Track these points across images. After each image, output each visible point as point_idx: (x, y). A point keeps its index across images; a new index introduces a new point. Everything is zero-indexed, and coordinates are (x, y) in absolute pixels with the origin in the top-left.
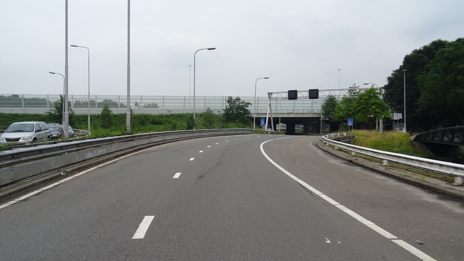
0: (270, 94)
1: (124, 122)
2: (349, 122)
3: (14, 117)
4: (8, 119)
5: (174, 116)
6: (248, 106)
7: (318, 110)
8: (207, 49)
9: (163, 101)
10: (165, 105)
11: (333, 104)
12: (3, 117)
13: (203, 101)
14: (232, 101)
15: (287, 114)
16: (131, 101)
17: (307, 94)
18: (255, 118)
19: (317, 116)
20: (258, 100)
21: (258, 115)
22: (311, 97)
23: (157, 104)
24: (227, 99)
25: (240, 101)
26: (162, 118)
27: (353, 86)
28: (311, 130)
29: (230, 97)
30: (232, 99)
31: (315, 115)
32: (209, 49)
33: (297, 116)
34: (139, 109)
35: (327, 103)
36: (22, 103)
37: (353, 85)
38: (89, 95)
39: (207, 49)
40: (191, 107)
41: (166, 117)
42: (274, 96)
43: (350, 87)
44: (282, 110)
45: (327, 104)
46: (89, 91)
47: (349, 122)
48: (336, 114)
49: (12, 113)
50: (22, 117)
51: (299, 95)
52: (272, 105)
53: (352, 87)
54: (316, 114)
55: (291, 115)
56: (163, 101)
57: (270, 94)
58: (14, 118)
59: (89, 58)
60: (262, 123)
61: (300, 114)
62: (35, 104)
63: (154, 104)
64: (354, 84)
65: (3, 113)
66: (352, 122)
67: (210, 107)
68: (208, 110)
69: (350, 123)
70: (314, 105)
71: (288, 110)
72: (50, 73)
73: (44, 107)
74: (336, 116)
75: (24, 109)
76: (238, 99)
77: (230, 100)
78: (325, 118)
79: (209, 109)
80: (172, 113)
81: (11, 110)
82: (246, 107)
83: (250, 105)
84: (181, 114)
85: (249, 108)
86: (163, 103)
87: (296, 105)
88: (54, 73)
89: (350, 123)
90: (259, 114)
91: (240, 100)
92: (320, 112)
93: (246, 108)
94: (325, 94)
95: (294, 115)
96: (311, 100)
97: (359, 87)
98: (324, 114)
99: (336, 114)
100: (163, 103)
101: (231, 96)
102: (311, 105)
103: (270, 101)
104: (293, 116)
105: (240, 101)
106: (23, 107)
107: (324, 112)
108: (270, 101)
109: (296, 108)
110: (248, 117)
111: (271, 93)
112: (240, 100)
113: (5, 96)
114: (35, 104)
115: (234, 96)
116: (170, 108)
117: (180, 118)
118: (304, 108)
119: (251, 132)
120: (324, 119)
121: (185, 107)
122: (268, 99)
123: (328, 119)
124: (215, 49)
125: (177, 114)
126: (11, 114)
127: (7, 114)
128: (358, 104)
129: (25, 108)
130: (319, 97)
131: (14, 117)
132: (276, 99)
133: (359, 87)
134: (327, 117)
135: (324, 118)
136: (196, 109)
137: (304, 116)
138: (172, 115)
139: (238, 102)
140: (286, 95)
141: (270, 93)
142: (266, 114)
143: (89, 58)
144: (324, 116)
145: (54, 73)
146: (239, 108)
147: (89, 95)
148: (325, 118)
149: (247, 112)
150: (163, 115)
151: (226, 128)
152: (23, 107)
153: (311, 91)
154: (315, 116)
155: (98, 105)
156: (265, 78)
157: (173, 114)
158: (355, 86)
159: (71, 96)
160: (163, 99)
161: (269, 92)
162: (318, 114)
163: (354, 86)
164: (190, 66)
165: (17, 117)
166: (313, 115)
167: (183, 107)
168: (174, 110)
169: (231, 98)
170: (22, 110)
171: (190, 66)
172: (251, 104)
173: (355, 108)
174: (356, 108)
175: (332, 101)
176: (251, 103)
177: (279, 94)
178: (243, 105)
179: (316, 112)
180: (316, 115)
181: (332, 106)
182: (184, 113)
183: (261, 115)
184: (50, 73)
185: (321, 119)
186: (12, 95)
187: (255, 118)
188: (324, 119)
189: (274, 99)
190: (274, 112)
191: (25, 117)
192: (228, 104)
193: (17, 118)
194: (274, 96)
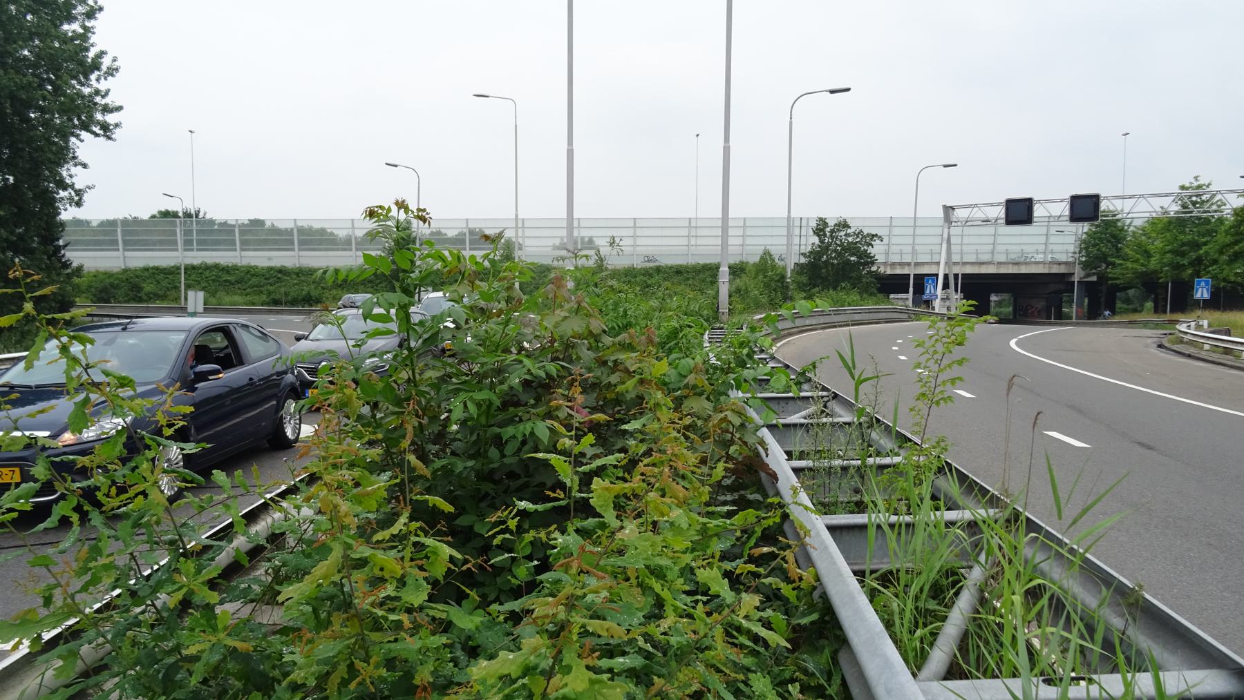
0: (948, 209)
1: (714, 282)
2: (1197, 289)
3: (279, 275)
4: (266, 279)
5: (665, 272)
6: (873, 243)
7: (1067, 252)
8: (826, 91)
9: (635, 231)
10: (639, 241)
11: (1114, 236)
12: (254, 275)
13: (685, 232)
14: (828, 229)
15: (972, 263)
16: (730, 233)
17: (1064, 209)
18: (914, 275)
19: (1062, 270)
20: (523, 227)
21: (889, 267)
22: (1010, 221)
23: (594, 239)
24: (814, 224)
25: (849, 231)
26: (635, 277)
27: (1191, 183)
28: (1039, 311)
29: (821, 219)
30: (826, 224)
31: (1055, 266)
32: (832, 92)
33: (1003, 270)
34: (621, 253)
35: (1095, 233)
36: (235, 240)
37: (1193, 181)
38: (915, 218)
39: (826, 91)
40: (698, 248)
41: (644, 275)
42: (960, 214)
43: (1183, 188)
44: (1052, 252)
45: (1096, 236)
46: (517, 210)
47: (1200, 289)
48: (1129, 265)
49: (273, 264)
50: (297, 274)
51: (1038, 211)
52: (953, 240)
53: (1187, 185)
54: (1059, 264)
55: (984, 266)
56: (635, 231)
57: (948, 209)
58: (279, 278)
59: (516, 126)
60: (928, 292)
61: (1011, 266)
62: (321, 242)
63: (587, 239)
64: (1196, 178)
65: (253, 264)
66: (1207, 290)
67: (769, 248)
68: (765, 254)
69: (1202, 292)
70: (1052, 239)
71: (1007, 253)
72: (387, 164)
73: (345, 250)
74: (1127, 269)
75: (124, 257)
76: (844, 225)
77: (821, 228)
78: (1088, 275)
79: (767, 253)
80: (657, 264)
81: (270, 259)
82: (868, 246)
83: (878, 242)
84: (681, 266)
85: (877, 250)
86: (634, 237)
87: (999, 240)
88: (396, 166)
89: (1202, 292)
90: (893, 264)
91: (850, 227)
92: (1071, 260)
93: (866, 248)
94: (1050, 210)
95: (992, 266)
96: (1075, 224)
97: (1209, 184)
98: (1085, 266)
99: (1129, 265)
100: (634, 237)
101: (823, 217)
102: (1043, 240)
103: (949, 228)
104: (991, 270)
105: (849, 231)
106: (468, 249)
107: (1084, 259)
108: (949, 228)
109: (999, 248)
110: (870, 272)
111: (953, 208)
112: (850, 227)
113: (229, 222)
114: (276, 242)
115: (832, 217)
116: (650, 251)
117: (681, 278)
118: (1009, 248)
119: (905, 316)
120: (1084, 278)
121: (638, 248)
122: (941, 222)
123: (1094, 278)
124: (848, 90)
125: (671, 268)
126: (271, 269)
127: (263, 268)
128: (1232, 235)
129: (302, 253)
130: (1035, 220)
131: (279, 275)
132: (967, 222)
133: (1209, 184)
134: (1094, 274)
135: (1082, 276)
136: (729, 253)
137: (1024, 270)
138: (658, 270)
139: (842, 233)
140: (1000, 212)
141: (950, 207)
142: (938, 263)
143: (516, 126)
144: (1083, 270)
145: (396, 166)
146: (852, 248)
147: (915, 218)
148: (1088, 275)
149: (868, 260)
150: (634, 269)
151: (849, 305)
152: (468, 249)
153: (1075, 200)
154: (1055, 270)
155: (357, 244)
156: (945, 166)
157: (660, 266)
158: (1198, 183)
159: (351, 221)
160: (635, 227)
161: (948, 205)
162: (1066, 263)
163: (1196, 184)
164: (698, 135)
165: (285, 274)
166: (1050, 268)
167: (632, 248)
168: (662, 255)
169: (823, 222)
170: (119, 257)
171: (698, 135)
172: (880, 237)
173: (1222, 249)
174: (1228, 248)
175: (1110, 226)
176: (879, 234)
177: (976, 209)
178: (858, 240)
179: (1063, 258)
180: (1058, 266)
181: (1109, 241)
182: (690, 262)
183: (898, 267)
184: (387, 164)
185: (1076, 280)
186: (249, 220)
187: (914, 275)
188: (1084, 278)
189: (959, 224)
190: (956, 258)
191: (303, 275)
192: (816, 240)
193: (285, 277)
194: (960, 214)
